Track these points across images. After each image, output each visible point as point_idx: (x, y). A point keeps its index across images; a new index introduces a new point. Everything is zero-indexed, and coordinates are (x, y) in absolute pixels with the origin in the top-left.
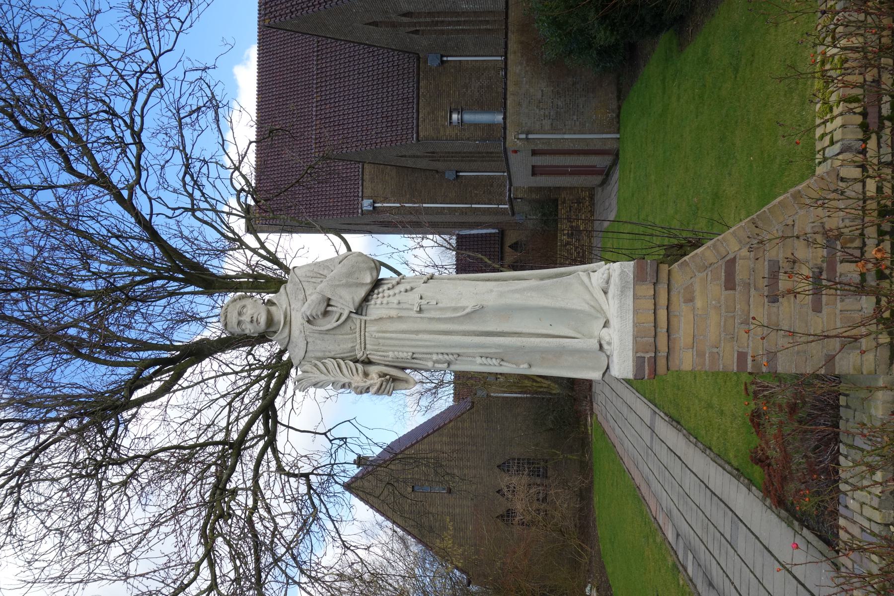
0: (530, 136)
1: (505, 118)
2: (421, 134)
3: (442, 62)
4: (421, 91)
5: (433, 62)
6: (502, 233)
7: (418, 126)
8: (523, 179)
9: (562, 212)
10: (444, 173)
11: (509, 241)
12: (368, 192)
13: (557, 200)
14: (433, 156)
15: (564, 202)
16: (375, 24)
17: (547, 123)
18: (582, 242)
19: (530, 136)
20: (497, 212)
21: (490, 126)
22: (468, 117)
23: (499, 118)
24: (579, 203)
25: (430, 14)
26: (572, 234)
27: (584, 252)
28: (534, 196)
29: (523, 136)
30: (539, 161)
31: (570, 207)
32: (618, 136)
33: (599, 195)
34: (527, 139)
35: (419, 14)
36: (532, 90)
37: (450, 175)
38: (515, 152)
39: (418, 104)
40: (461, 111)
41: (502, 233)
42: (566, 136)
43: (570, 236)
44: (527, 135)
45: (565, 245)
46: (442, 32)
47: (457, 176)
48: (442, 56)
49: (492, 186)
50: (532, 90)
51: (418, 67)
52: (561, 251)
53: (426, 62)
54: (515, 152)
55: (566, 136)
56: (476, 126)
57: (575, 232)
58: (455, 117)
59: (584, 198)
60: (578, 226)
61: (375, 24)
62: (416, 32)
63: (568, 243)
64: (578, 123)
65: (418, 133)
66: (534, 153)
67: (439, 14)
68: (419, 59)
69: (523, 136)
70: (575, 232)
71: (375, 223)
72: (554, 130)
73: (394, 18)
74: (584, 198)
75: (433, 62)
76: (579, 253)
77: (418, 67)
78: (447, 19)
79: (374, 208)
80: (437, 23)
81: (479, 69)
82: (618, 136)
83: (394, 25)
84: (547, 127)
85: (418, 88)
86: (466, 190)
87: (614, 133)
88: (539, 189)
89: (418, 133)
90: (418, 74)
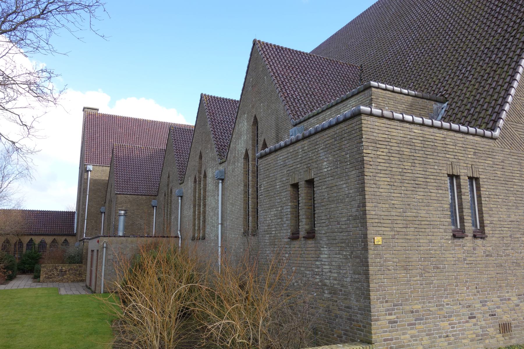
0: (105, 249)
1: (120, 236)
2: (119, 196)
3: (154, 207)
4: (141, 196)
5: (154, 202)
6: (74, 235)
7: (123, 194)
8: (92, 245)
9: (75, 266)
10: (104, 206)
11: (69, 239)
12: (97, 168)
13: (82, 263)
14: (111, 201)
15: (80, 267)
16: (169, 177)
17: (111, 257)
18: (57, 277)
19: (105, 249)
20: (82, 232)
21: (116, 229)
22: (122, 218)
23: (121, 234)
24: (79, 274)
25: (171, 201)
26: (62, 272)
27: (51, 278)
28: (84, 251)
29: (105, 245)
30: (95, 253)
31: (77, 270)
32: (102, 292)
33: (82, 284)
34: (103, 247)
35: (171, 197)
36: (128, 249)
37: (103, 209)
38: (98, 242)
39: (134, 195)
40: (125, 215)
41: (74, 235)
42: (103, 267)
43: (61, 271)
44: (106, 247)
45: (55, 268)
46: (164, 207)
47: (102, 213)
48: (156, 207)
49: (96, 230)
50: (128, 249)
51: (152, 196)
52: (53, 266)
53: (154, 199)
54: (98, 242)
55: (103, 267)
56: (117, 221)
57: (63, 273)
58: (123, 212)
59: (81, 277)
60: (66, 274)
61: (169, 177)
62: (165, 195)
63: (57, 269)
64: (110, 272)
65: (120, 194)
66: (98, 251)
67: (171, 206)
68: (155, 196)
69: (105, 245)
70: (63, 273)
71: (82, 171)
72: (107, 260)
73: (170, 185)
74: (81, 277)
75: (154, 202)
76: (51, 275)
77: (152, 196)
78: (250, 218)
79: (88, 171)
80: (168, 205)
81: (149, 224)
82: (102, 292)
83: (168, 185)
84: (109, 257)
85: (141, 195)
86: (94, 217)
87: (104, 290)
88: (87, 253)
89: (120, 194)
90: (148, 195)
